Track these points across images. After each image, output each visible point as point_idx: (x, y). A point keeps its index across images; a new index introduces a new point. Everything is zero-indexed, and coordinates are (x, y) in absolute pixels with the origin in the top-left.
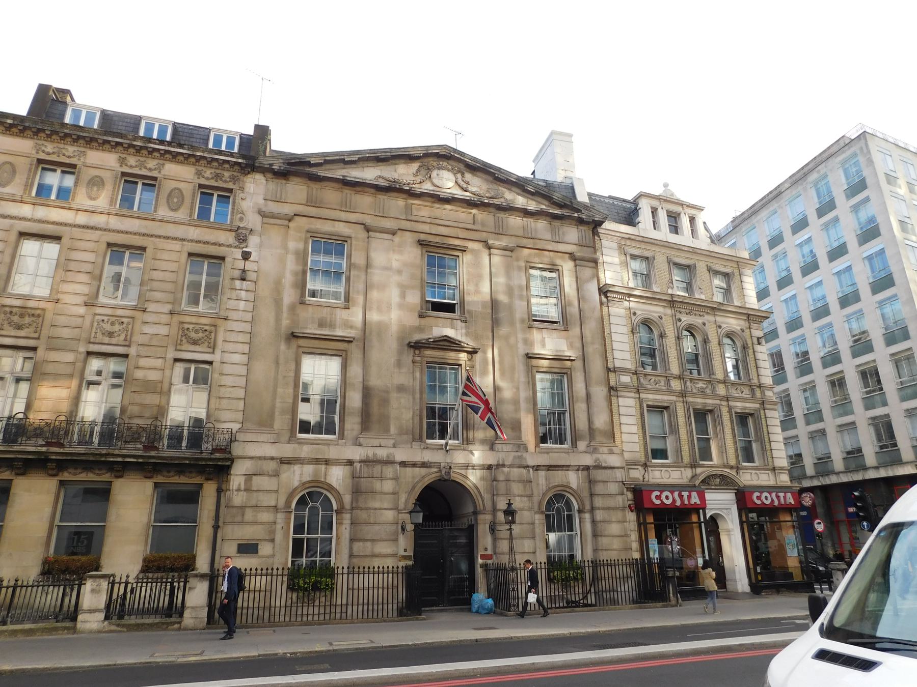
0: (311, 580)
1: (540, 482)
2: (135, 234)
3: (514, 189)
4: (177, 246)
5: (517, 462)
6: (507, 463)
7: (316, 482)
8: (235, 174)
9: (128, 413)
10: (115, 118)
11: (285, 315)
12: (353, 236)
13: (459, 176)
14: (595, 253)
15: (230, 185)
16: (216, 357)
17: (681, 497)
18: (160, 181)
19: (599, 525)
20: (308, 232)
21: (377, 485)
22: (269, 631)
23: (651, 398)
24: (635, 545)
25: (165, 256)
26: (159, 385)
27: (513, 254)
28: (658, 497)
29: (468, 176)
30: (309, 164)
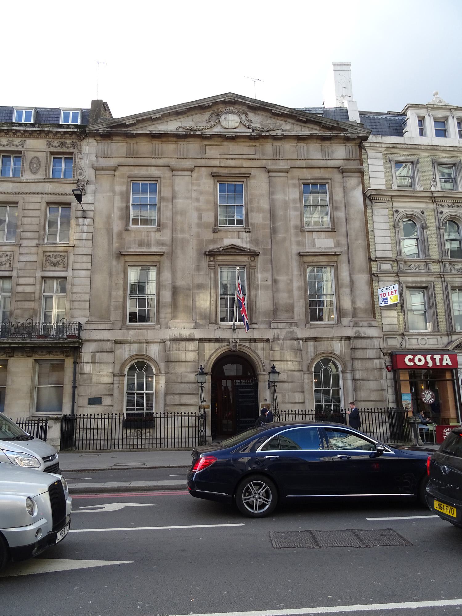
0: (139, 420)
1: (309, 350)
2: (10, 193)
3: (289, 120)
4: (38, 199)
5: (289, 336)
6: (281, 337)
7: (139, 355)
8: (74, 141)
9: (14, 315)
10: (330, 112)
11: (115, 240)
12: (162, 176)
13: (243, 117)
14: (361, 164)
15: (71, 150)
16: (69, 274)
17: (433, 360)
18: (24, 153)
19: (358, 382)
20: (128, 177)
21: (183, 356)
22: (95, 455)
23: (410, 280)
24: (391, 398)
25: (31, 206)
26: (33, 295)
27: (289, 175)
28: (410, 360)
29: (251, 116)
30: (125, 126)
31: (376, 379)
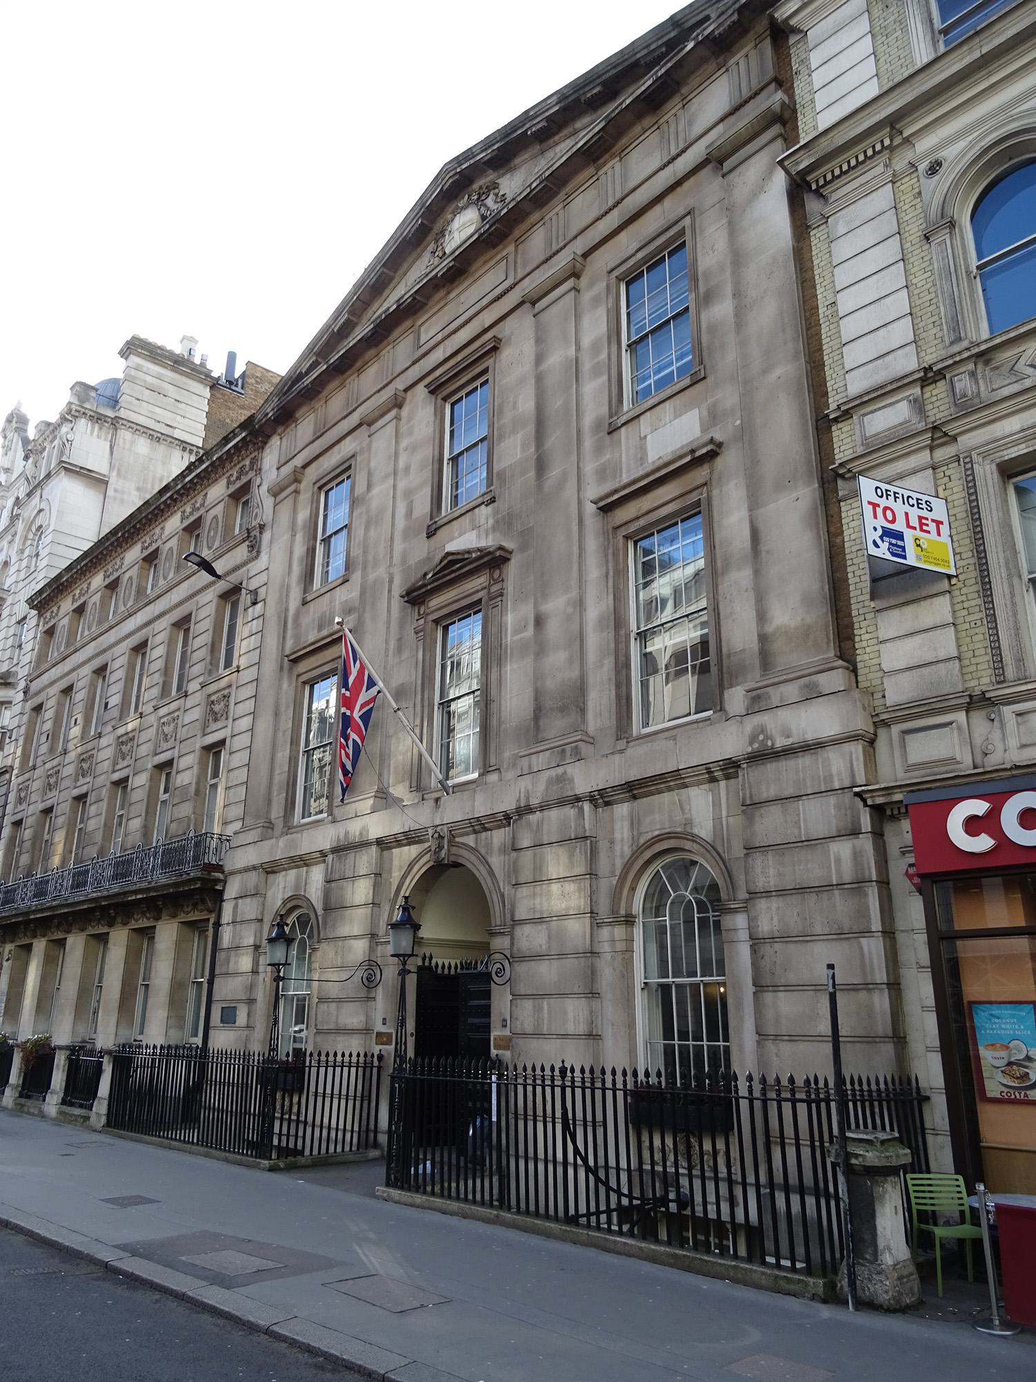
1: (618, 836)
5: (555, 794)
6: (534, 801)
31: (840, 935)
